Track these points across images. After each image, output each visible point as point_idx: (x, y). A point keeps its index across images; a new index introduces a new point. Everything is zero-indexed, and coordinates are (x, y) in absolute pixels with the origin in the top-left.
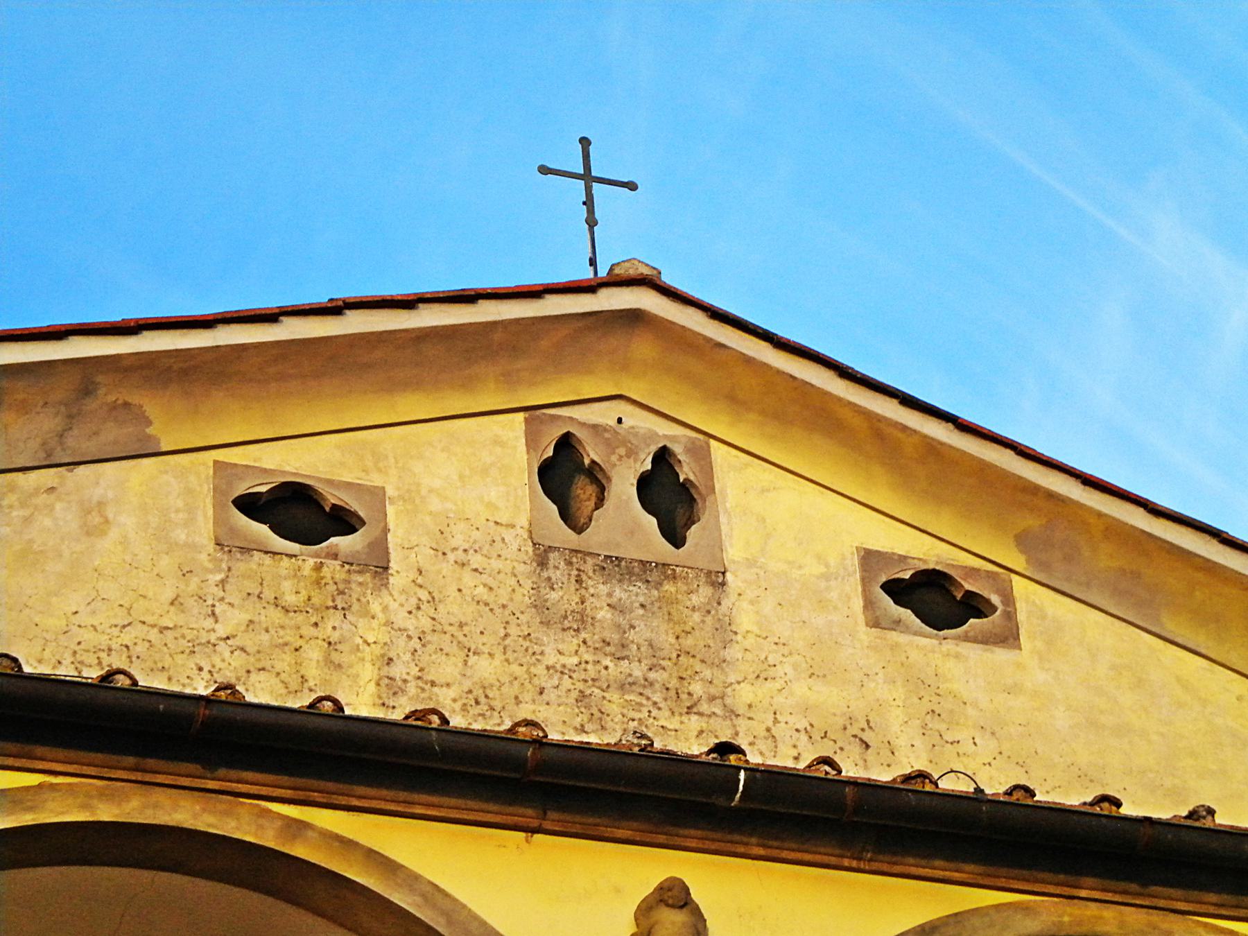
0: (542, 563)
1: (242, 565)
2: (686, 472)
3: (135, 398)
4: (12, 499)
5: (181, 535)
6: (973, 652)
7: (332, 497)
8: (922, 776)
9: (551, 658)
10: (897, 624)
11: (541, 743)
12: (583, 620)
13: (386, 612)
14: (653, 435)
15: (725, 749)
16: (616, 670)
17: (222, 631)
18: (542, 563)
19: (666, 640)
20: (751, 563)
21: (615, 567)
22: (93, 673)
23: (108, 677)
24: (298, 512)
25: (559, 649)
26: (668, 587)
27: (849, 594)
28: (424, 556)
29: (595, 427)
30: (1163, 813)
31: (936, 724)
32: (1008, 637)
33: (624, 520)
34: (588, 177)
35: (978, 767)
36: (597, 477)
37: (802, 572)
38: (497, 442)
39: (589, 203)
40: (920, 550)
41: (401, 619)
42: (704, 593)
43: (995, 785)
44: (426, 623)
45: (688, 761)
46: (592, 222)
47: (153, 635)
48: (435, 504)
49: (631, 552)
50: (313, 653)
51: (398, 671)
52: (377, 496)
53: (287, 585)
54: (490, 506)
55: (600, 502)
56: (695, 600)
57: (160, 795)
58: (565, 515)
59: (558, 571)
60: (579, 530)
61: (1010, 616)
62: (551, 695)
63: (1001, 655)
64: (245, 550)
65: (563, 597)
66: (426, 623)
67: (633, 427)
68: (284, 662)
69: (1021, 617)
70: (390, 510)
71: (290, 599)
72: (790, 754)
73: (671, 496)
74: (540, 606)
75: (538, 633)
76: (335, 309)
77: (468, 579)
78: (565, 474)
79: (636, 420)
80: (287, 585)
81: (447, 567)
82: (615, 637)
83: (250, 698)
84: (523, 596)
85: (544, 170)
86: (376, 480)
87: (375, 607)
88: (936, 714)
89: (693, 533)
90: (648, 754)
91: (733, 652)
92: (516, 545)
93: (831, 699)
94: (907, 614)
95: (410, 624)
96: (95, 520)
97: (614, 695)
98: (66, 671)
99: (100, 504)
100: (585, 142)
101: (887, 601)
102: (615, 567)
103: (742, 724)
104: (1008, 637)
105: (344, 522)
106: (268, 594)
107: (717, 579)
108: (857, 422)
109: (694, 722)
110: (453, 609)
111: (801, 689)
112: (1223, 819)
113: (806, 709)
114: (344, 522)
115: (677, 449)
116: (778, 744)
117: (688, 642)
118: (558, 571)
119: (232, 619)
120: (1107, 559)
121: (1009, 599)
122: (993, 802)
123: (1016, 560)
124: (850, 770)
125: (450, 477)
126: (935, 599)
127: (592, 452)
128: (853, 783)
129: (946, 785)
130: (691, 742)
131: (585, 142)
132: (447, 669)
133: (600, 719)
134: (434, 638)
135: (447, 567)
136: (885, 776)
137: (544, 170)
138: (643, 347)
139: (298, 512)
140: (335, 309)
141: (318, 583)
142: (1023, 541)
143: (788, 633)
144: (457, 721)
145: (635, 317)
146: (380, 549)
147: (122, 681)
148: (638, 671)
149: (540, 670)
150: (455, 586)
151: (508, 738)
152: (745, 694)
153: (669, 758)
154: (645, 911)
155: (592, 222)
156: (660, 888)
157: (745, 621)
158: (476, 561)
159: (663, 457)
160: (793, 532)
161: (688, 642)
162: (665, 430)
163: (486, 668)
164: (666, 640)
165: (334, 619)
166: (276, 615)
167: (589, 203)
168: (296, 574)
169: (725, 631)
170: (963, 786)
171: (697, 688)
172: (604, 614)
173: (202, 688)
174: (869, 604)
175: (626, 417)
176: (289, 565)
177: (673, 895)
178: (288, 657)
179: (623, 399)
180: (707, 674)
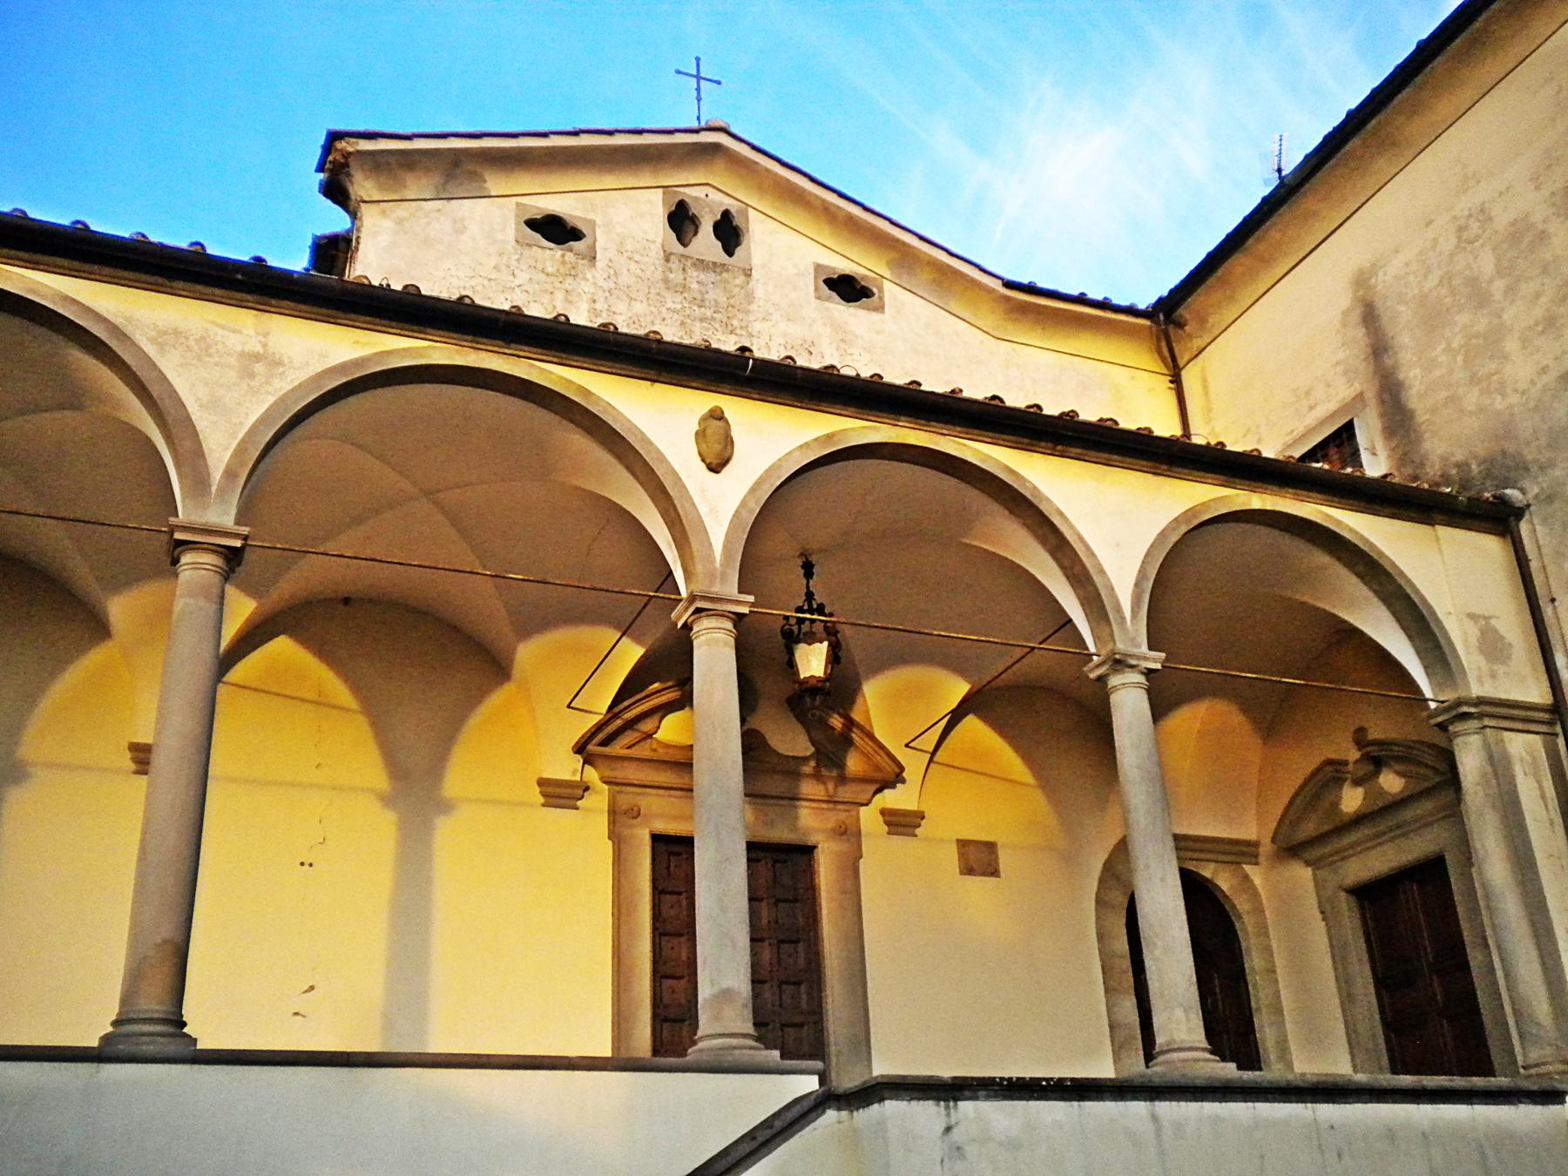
0: (667, 260)
1: (527, 252)
2: (737, 221)
3: (479, 169)
4: (420, 214)
5: (499, 236)
6: (862, 313)
7: (572, 222)
8: (833, 367)
9: (670, 305)
10: (829, 299)
11: (660, 342)
12: (685, 288)
13: (597, 275)
14: (722, 204)
15: (743, 349)
16: (698, 312)
17: (517, 282)
18: (667, 260)
19: (723, 299)
20: (764, 266)
21: (701, 264)
22: (454, 297)
23: (462, 298)
24: (555, 230)
25: (673, 301)
26: (725, 275)
27: (808, 283)
28: (612, 254)
29: (696, 198)
30: (940, 390)
31: (843, 346)
32: (880, 308)
33: (706, 243)
34: (698, 77)
35: (858, 365)
36: (695, 222)
37: (1157, 881)
38: (650, 202)
39: (698, 89)
40: (843, 266)
41: (601, 282)
42: (741, 280)
43: (865, 373)
44: (612, 285)
45: (726, 353)
46: (699, 99)
47: (486, 282)
48: (619, 230)
49: (710, 258)
50: (560, 295)
51: (598, 306)
52: (593, 223)
53: (548, 264)
54: (645, 232)
55: (696, 233)
56: (738, 282)
57: (484, 354)
58: (679, 239)
59: (675, 264)
60: (685, 245)
61: (881, 298)
62: (668, 321)
63: (875, 316)
64: (529, 245)
65: (676, 277)
66: (612, 285)
67: (1513, 224)
68: (546, 298)
69: (886, 299)
70: (598, 231)
71: (550, 270)
72: (775, 355)
73: (729, 233)
74: (666, 281)
75: (665, 293)
76: (576, 133)
77: (633, 266)
78: (681, 220)
79: (715, 196)
80: (548, 264)
81: (623, 259)
82: (699, 297)
83: (526, 312)
84: (658, 275)
85: (678, 72)
86: (591, 216)
87: (589, 276)
88: (844, 339)
89: (738, 251)
90: (708, 349)
91: (753, 307)
92: (656, 253)
93: (797, 331)
94: (834, 294)
95: (605, 285)
96: (459, 228)
97: (697, 324)
98: (444, 295)
99: (462, 220)
100: (698, 59)
101: (825, 288)
102: (701, 264)
103: (755, 340)
104: (880, 308)
105: (576, 235)
106: (540, 266)
107: (748, 273)
108: (817, 203)
109: (733, 338)
110: (625, 279)
111: (783, 326)
112: (965, 394)
113: (785, 335)
114: (576, 235)
115: (733, 211)
116: (769, 349)
117: (732, 301)
118: (675, 264)
119: (522, 277)
120: (926, 275)
121: (881, 290)
122: (864, 380)
123: (887, 274)
124: (800, 362)
125: (626, 215)
126: (848, 289)
127: (694, 210)
128: (802, 368)
129: (844, 371)
130: (729, 345)
131: (698, 59)
132: (621, 307)
133: (690, 333)
134: (616, 292)
135: (623, 259)
136: (816, 366)
137: (678, 72)
138: (720, 164)
139: (555, 230)
140: (576, 133)
141: (564, 263)
142: (891, 265)
143: (783, 315)
144: (623, 329)
145: (716, 147)
146: (593, 248)
147: (467, 301)
148: (709, 313)
149: (664, 310)
150: (624, 272)
151: (646, 338)
152: (757, 327)
153: (718, 351)
154: (703, 419)
155: (699, 99)
156: (711, 411)
157: (759, 293)
158: (637, 257)
159: (726, 214)
160: (785, 251)
161: (732, 301)
162: (728, 203)
163: (639, 307)
164: (723, 299)
165: (569, 280)
166: (542, 277)
167: (698, 89)
168: (553, 259)
169: (750, 297)
170: (850, 372)
171: (735, 323)
172: (695, 286)
173: (506, 307)
174: (817, 289)
175: (711, 193)
176: (550, 254)
177: (717, 415)
178: (548, 296)
179: (705, 183)
180: (740, 316)
